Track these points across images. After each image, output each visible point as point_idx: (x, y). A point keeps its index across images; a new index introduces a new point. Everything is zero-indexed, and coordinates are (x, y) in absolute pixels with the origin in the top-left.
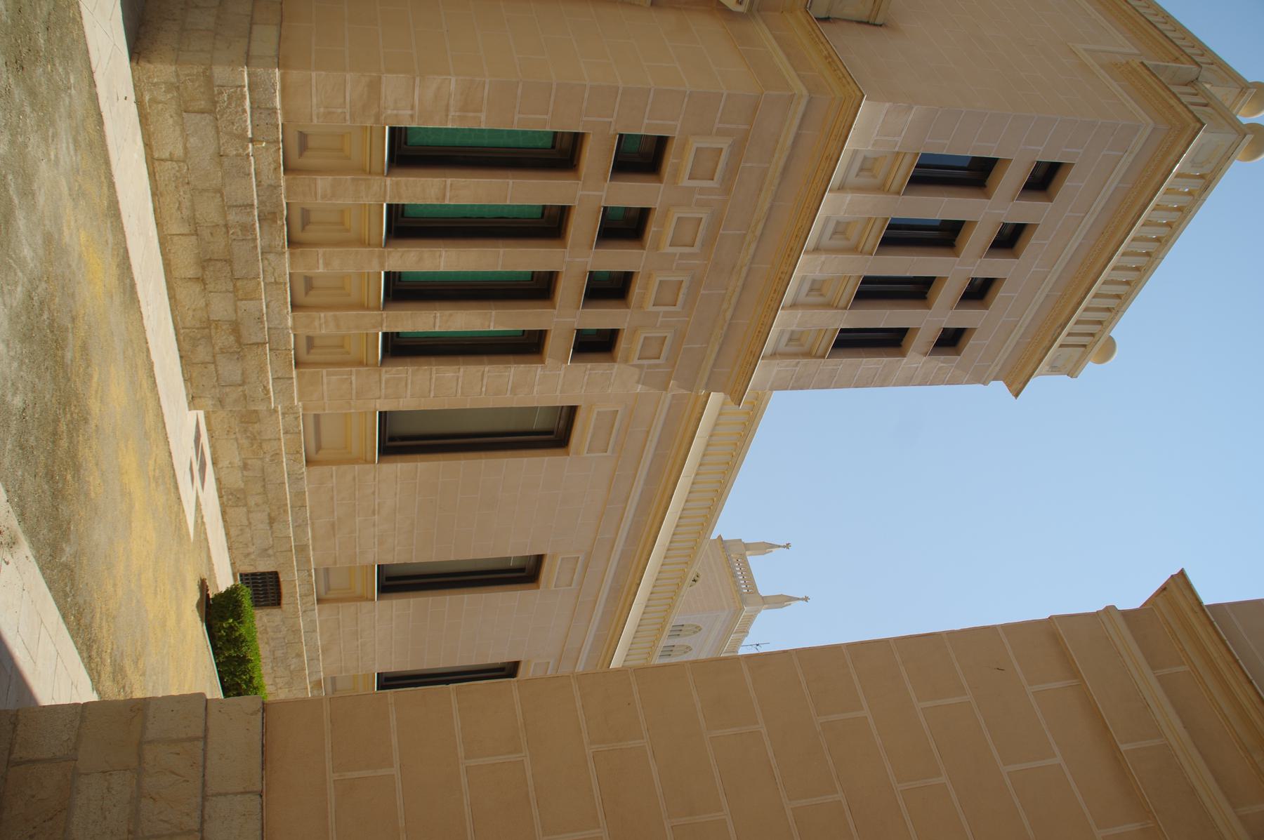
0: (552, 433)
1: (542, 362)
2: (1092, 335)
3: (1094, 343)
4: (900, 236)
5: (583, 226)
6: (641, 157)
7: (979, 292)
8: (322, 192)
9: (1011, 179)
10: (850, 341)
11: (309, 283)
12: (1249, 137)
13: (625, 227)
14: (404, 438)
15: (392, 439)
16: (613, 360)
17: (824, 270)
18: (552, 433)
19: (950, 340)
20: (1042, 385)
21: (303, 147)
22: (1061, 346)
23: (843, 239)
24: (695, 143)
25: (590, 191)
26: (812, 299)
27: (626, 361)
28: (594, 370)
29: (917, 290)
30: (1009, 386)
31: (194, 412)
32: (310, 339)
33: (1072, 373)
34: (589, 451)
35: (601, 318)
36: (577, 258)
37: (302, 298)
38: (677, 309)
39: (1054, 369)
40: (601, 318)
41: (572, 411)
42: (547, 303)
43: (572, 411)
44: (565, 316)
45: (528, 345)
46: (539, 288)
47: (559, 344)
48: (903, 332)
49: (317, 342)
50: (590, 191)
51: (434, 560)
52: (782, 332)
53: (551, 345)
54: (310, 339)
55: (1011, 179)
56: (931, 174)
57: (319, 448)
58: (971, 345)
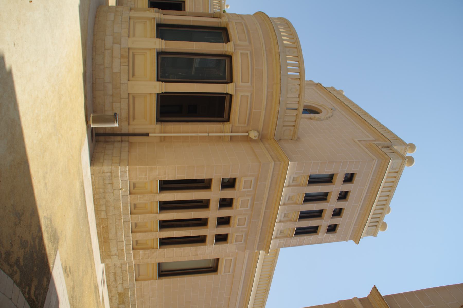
0: (212, 268)
1: (208, 228)
2: (378, 222)
3: (378, 225)
4: (304, 216)
5: (214, 204)
6: (229, 184)
7: (343, 196)
8: (140, 200)
9: (339, 179)
10: (300, 232)
11: (136, 225)
12: (407, 160)
13: (226, 203)
14: (165, 271)
15: (162, 272)
16: (228, 243)
17: (285, 217)
18: (212, 268)
19: (332, 229)
20: (365, 240)
21: (134, 187)
22: (369, 226)
23: (295, 183)
24: (244, 179)
25: (215, 194)
26: (280, 236)
27: (231, 243)
28: (221, 246)
29: (318, 214)
30: (355, 241)
31: (102, 264)
32: (135, 205)
33: (375, 235)
34: (224, 273)
35: (223, 230)
36: (213, 214)
37: (134, 230)
38: (245, 226)
39: (368, 234)
40: (223, 230)
41: (218, 260)
42: (207, 209)
43: (218, 260)
44: (211, 231)
45: (201, 240)
46: (203, 223)
47: (210, 239)
48: (321, 211)
49: (139, 242)
50: (215, 194)
51: (179, 261)
52: (278, 230)
53: (208, 239)
54: (135, 205)
55: (339, 179)
56: (313, 181)
57: (139, 275)
58: (339, 229)
